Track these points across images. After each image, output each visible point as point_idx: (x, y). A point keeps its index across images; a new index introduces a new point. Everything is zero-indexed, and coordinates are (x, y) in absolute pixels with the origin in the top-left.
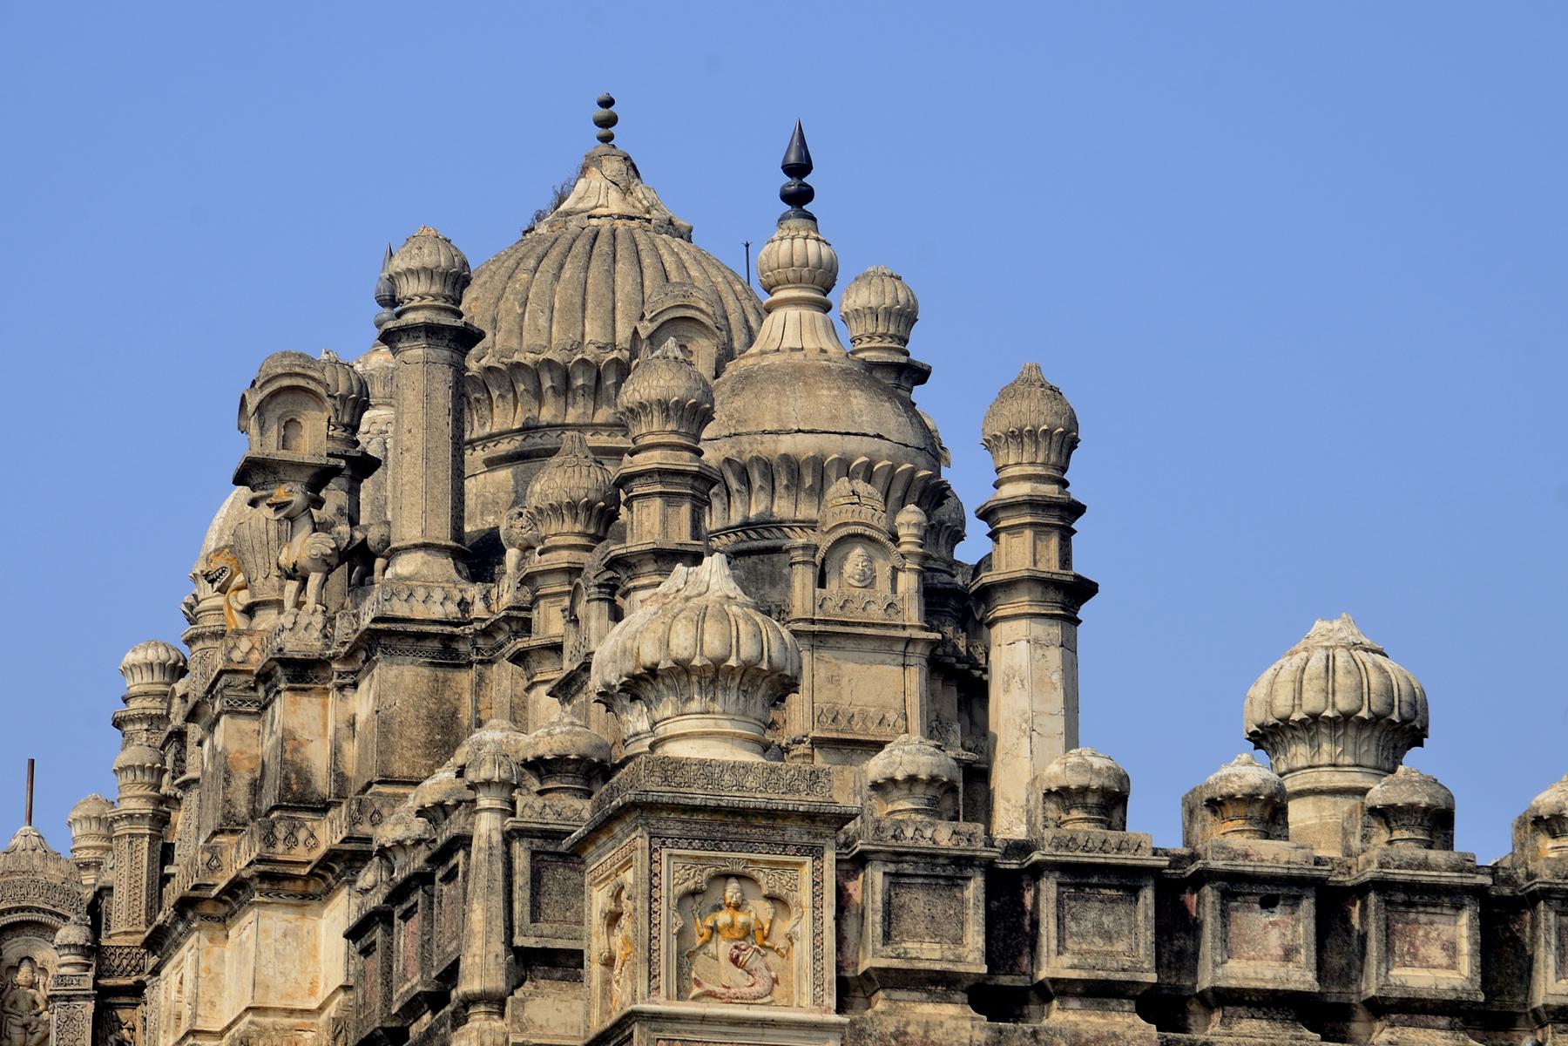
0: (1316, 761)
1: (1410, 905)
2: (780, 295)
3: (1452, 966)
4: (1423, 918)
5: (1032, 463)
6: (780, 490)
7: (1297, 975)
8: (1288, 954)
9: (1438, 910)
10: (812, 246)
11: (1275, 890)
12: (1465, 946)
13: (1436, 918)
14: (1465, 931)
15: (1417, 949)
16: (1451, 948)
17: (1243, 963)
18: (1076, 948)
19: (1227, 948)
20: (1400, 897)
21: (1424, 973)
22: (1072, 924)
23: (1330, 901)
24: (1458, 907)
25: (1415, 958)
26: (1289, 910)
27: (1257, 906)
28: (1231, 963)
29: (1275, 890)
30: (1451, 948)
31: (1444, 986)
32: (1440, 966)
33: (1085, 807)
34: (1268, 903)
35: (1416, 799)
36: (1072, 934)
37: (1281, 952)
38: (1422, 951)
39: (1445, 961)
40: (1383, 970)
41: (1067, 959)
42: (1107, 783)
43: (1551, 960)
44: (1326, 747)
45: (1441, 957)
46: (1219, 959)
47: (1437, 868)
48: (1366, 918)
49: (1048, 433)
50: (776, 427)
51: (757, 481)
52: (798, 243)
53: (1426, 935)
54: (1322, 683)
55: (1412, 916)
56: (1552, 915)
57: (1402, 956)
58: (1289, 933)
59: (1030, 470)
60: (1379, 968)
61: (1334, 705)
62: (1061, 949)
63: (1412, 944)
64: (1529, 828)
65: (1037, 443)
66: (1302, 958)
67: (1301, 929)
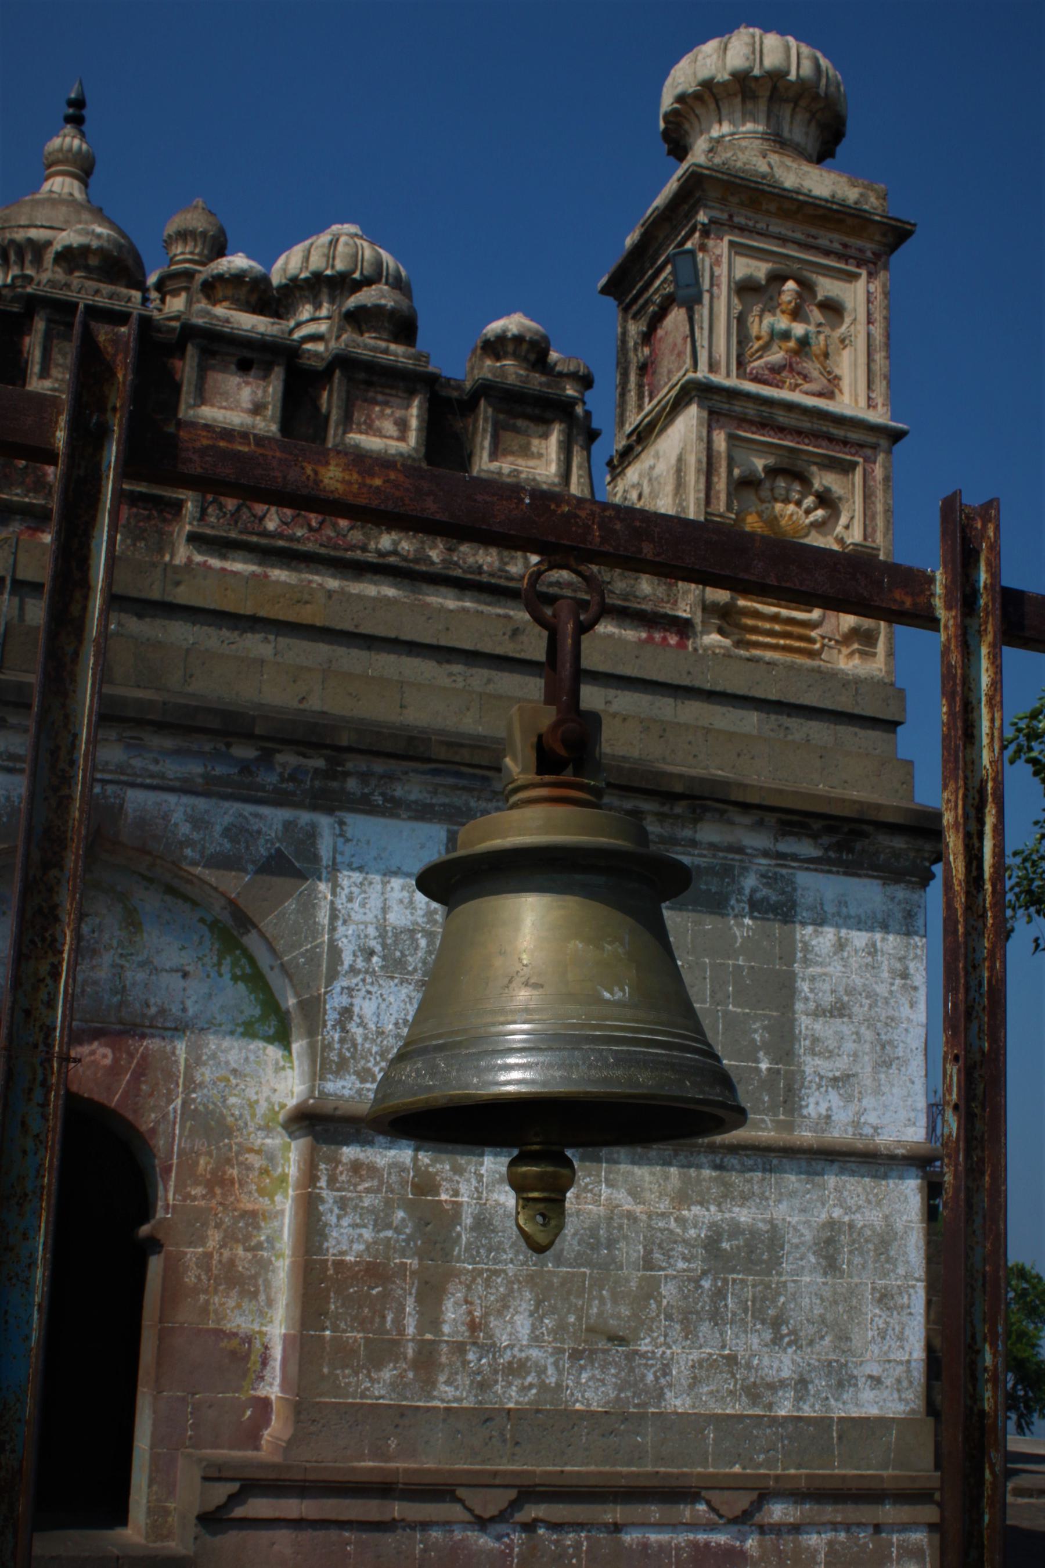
0: (317, 314)
1: (369, 384)
2: (53, 169)
3: (402, 438)
4: (380, 398)
5: (192, 253)
6: (27, 264)
7: (262, 425)
8: (257, 409)
9: (394, 392)
10: (76, 142)
11: (251, 356)
12: (414, 423)
13: (392, 399)
14: (414, 411)
15: (373, 421)
16: (402, 425)
17: (215, 410)
18: (60, 376)
19: (201, 398)
20: (362, 376)
21: (377, 440)
22: (59, 356)
23: (304, 387)
24: (411, 393)
25: (370, 428)
26: (262, 374)
27: (233, 367)
28: (204, 408)
29: (251, 356)
30: (402, 425)
31: (392, 451)
32: (391, 437)
33: (87, 268)
34: (244, 367)
35: (383, 302)
36: (58, 365)
37: (250, 406)
38: (377, 423)
39: (395, 434)
40: (340, 431)
41: (47, 384)
42: (105, 244)
43: (487, 444)
44: (326, 305)
45: (391, 433)
46: (192, 401)
47: (396, 355)
48: (330, 400)
49: (204, 234)
50: (27, 223)
51: (13, 257)
52: (68, 140)
53: (382, 411)
54: (326, 250)
55: (371, 394)
56: (490, 410)
57: (359, 424)
58: (260, 393)
59: (189, 257)
60: (336, 430)
61: (333, 267)
62: (44, 374)
63: (369, 416)
64: (479, 351)
65: (195, 240)
66: (269, 413)
67: (271, 390)
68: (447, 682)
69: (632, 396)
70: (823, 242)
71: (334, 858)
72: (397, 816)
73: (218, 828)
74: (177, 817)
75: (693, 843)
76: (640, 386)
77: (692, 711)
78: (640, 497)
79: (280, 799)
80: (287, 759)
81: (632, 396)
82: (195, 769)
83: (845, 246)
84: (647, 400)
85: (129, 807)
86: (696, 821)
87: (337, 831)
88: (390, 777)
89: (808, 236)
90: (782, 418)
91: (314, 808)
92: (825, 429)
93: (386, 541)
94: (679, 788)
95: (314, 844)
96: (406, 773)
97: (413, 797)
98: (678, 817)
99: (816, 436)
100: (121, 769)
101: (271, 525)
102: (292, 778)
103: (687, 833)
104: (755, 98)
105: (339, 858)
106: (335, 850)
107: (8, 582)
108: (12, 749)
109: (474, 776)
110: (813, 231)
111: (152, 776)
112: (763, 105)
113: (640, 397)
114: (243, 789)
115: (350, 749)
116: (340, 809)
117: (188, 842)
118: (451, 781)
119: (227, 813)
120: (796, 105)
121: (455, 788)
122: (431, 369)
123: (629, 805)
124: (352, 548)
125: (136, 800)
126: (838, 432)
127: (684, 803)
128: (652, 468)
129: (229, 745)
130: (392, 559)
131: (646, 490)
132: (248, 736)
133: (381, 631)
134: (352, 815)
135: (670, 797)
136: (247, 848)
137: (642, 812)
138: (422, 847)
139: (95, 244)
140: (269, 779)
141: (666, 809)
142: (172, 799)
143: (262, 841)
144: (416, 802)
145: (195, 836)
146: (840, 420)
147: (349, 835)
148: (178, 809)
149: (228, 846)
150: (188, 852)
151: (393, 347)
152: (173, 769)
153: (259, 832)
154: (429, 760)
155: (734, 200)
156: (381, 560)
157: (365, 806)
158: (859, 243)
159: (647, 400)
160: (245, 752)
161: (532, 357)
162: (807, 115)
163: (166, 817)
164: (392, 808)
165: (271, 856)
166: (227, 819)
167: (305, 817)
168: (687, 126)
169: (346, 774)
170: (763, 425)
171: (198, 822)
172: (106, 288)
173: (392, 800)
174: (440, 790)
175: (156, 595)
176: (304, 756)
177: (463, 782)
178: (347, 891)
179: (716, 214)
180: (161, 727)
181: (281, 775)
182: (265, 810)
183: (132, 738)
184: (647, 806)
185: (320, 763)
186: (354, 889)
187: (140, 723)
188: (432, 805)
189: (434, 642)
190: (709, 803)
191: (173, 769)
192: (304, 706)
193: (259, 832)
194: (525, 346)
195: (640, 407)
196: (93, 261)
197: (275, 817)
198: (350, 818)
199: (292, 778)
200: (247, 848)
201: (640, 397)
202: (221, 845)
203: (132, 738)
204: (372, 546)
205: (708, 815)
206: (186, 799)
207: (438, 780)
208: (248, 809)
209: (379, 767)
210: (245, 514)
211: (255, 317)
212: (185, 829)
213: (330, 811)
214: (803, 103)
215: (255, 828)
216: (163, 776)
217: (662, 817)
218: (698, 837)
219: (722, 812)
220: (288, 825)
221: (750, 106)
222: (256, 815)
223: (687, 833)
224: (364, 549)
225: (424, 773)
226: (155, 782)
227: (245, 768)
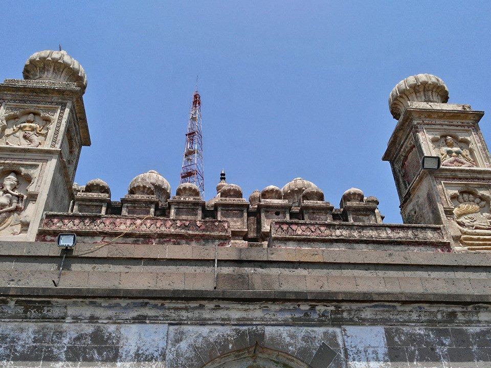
0: (294, 201)
4: (317, 216)
68: (370, 275)
69: (402, 185)
70: (455, 123)
71: (344, 344)
72: (363, 325)
73: (300, 338)
74: (284, 335)
75: (479, 322)
76: (404, 182)
77: (460, 275)
78: (415, 213)
79: (320, 324)
80: (320, 308)
81: (402, 185)
82: (288, 316)
83: (463, 123)
84: (408, 185)
85: (267, 333)
86: (477, 313)
87: (343, 334)
88: (359, 310)
89: (449, 122)
90: (460, 175)
91: (333, 325)
92: (475, 176)
93: (338, 232)
94: (469, 300)
95: (336, 340)
96: (365, 308)
97: (368, 317)
98: (470, 312)
99: (473, 179)
100: (262, 319)
101: (299, 232)
102: (323, 315)
103: (475, 318)
104: (419, 92)
105: (346, 344)
106: (344, 341)
107: (216, 261)
108: (223, 317)
109: (389, 306)
110: (451, 121)
111: (273, 321)
112: (422, 93)
113: (405, 185)
114: (305, 321)
115: (343, 301)
116: (343, 324)
117: (291, 344)
118: (381, 309)
119: (303, 331)
120: (432, 91)
121: (383, 311)
122: (331, 205)
123: (450, 310)
124: (327, 236)
125: (269, 331)
126: (480, 176)
127: (471, 306)
128: (417, 202)
129: (299, 305)
130: (341, 237)
131: (417, 210)
132: (306, 300)
133: (343, 261)
134: (348, 327)
135: (466, 304)
136: (312, 344)
137: (455, 312)
138: (376, 336)
139: (232, 188)
140: (315, 316)
141: (465, 309)
142: (281, 328)
143: (316, 341)
144: (370, 319)
145: (292, 342)
146: (480, 172)
147: (348, 334)
148: (284, 331)
149: (305, 344)
150: (290, 348)
151: (318, 202)
152: (281, 317)
153: (315, 337)
154: (373, 301)
155: (423, 116)
156: (338, 238)
157: (352, 322)
158: (467, 121)
159: (408, 185)
160: (305, 307)
161: (359, 199)
162: (437, 94)
163: (280, 336)
164: (362, 322)
165: (321, 346)
166: (303, 334)
167: (331, 330)
168: (399, 107)
169: (343, 311)
170: (454, 178)
171: (292, 336)
172: (236, 199)
173: (361, 319)
174: (378, 313)
175: (265, 259)
176: (327, 306)
177: (386, 309)
178: (352, 356)
179: (419, 121)
180: (274, 301)
181: (319, 315)
182: (315, 329)
183: (264, 307)
184: (458, 309)
185: (333, 308)
186: (355, 355)
187: (267, 300)
188: (376, 319)
189: (363, 262)
190: (481, 304)
191: (281, 317)
192: (322, 289)
193: (315, 337)
194: (356, 196)
195: (406, 188)
196: (232, 193)
197: (320, 331)
198: (348, 328)
199: (323, 315)
200: (312, 344)
201: (405, 185)
202: (302, 344)
203: (264, 307)
204: (333, 234)
205: (482, 310)
206: (286, 328)
207: (377, 309)
208: (310, 329)
209: (354, 306)
210: (290, 230)
211: (278, 200)
212: (288, 339)
213: (339, 326)
214: (434, 90)
215: (313, 336)
216: (277, 320)
217: (464, 313)
218: (480, 319)
219: (487, 308)
220: (325, 333)
221: (418, 94)
222: (313, 331)
223: (475, 318)
224: (331, 236)
225: (371, 307)
226: (275, 323)
227: (306, 314)
